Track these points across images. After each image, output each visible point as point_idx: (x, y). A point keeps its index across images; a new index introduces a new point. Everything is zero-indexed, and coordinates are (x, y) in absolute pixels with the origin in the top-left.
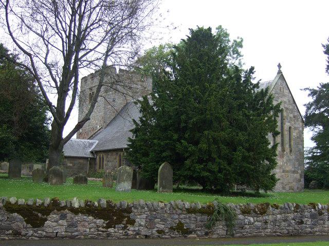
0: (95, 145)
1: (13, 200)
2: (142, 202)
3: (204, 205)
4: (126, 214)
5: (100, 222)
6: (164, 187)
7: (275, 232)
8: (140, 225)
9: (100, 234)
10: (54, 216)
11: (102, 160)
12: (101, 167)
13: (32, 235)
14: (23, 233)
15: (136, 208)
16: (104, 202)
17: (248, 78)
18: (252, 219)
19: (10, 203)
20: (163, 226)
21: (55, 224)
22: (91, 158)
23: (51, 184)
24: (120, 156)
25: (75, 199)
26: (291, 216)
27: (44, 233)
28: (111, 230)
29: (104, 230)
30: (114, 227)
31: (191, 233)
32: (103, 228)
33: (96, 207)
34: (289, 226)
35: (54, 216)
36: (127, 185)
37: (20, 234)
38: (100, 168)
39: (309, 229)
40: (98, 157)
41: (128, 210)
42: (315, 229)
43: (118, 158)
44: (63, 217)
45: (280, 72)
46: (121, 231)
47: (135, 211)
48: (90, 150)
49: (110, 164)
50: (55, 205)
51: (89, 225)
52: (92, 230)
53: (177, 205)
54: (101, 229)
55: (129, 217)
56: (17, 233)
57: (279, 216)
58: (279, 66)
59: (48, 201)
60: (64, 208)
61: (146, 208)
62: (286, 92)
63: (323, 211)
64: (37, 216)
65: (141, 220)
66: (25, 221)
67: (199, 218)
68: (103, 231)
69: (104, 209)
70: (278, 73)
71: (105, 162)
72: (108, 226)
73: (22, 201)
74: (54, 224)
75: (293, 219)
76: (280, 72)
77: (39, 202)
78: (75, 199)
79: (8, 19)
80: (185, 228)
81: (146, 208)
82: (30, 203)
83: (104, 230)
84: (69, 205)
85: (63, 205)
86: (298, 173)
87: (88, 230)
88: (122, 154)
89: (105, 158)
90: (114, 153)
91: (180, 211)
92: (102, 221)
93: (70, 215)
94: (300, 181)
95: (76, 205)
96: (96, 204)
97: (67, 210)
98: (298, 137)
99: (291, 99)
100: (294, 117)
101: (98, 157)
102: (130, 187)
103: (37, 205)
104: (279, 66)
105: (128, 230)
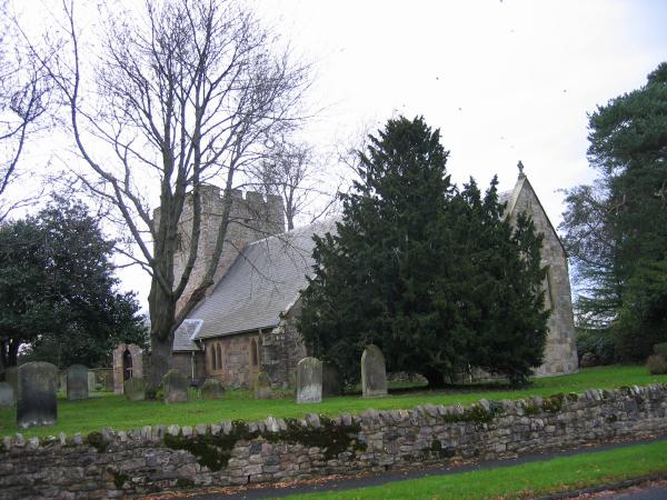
0: (198, 329)
1: (173, 430)
2: (374, 412)
3: (468, 408)
4: (351, 435)
5: (314, 451)
6: (373, 387)
7: (577, 438)
8: (376, 450)
9: (315, 472)
10: (241, 448)
11: (217, 354)
12: (217, 364)
13: (212, 484)
14: (197, 480)
15: (366, 423)
16: (315, 418)
17: (492, 194)
18: (541, 422)
19: (171, 435)
20: (410, 448)
21: (245, 462)
22: (196, 352)
23: (171, 402)
24: (254, 343)
25: (271, 418)
26: (598, 410)
27: (230, 479)
28: (332, 463)
29: (322, 463)
30: (337, 458)
31: (453, 455)
32: (320, 460)
33: (304, 428)
34: (597, 426)
35: (242, 449)
36: (313, 391)
37: (192, 485)
38: (214, 367)
39: (627, 429)
40: (209, 349)
41: (355, 428)
42: (636, 427)
43: (249, 347)
44: (256, 449)
45: (522, 176)
46: (347, 464)
47: (366, 428)
48: (193, 338)
49: (234, 359)
50: (241, 432)
51: (298, 460)
52: (303, 466)
53: (427, 413)
54: (316, 462)
55: (356, 439)
56: (185, 483)
57: (580, 412)
58: (520, 166)
59: (228, 428)
60: (255, 435)
61: (381, 422)
62: (535, 207)
63: (644, 397)
64: (215, 451)
65: (376, 440)
66: (199, 462)
67: (462, 429)
68: (319, 466)
69: (317, 431)
70: (519, 178)
71: (224, 357)
72: (328, 457)
73: (187, 430)
74: (247, 463)
75: (602, 415)
76: (522, 176)
77: (216, 429)
78: (271, 418)
79: (77, 121)
80: (443, 447)
81: (381, 422)
82: (203, 431)
83: (322, 463)
84: (262, 430)
85: (254, 429)
86: (566, 342)
87: (297, 467)
88: (257, 338)
89: (223, 350)
90: (242, 339)
91: (434, 421)
92: (317, 448)
93: (266, 446)
94: (571, 355)
95: (274, 428)
96: (304, 423)
97: (260, 438)
98: (560, 283)
99: (544, 219)
100: (552, 249)
101: (209, 349)
102: (320, 394)
103: (214, 433)
104: (520, 166)
105: (359, 460)
